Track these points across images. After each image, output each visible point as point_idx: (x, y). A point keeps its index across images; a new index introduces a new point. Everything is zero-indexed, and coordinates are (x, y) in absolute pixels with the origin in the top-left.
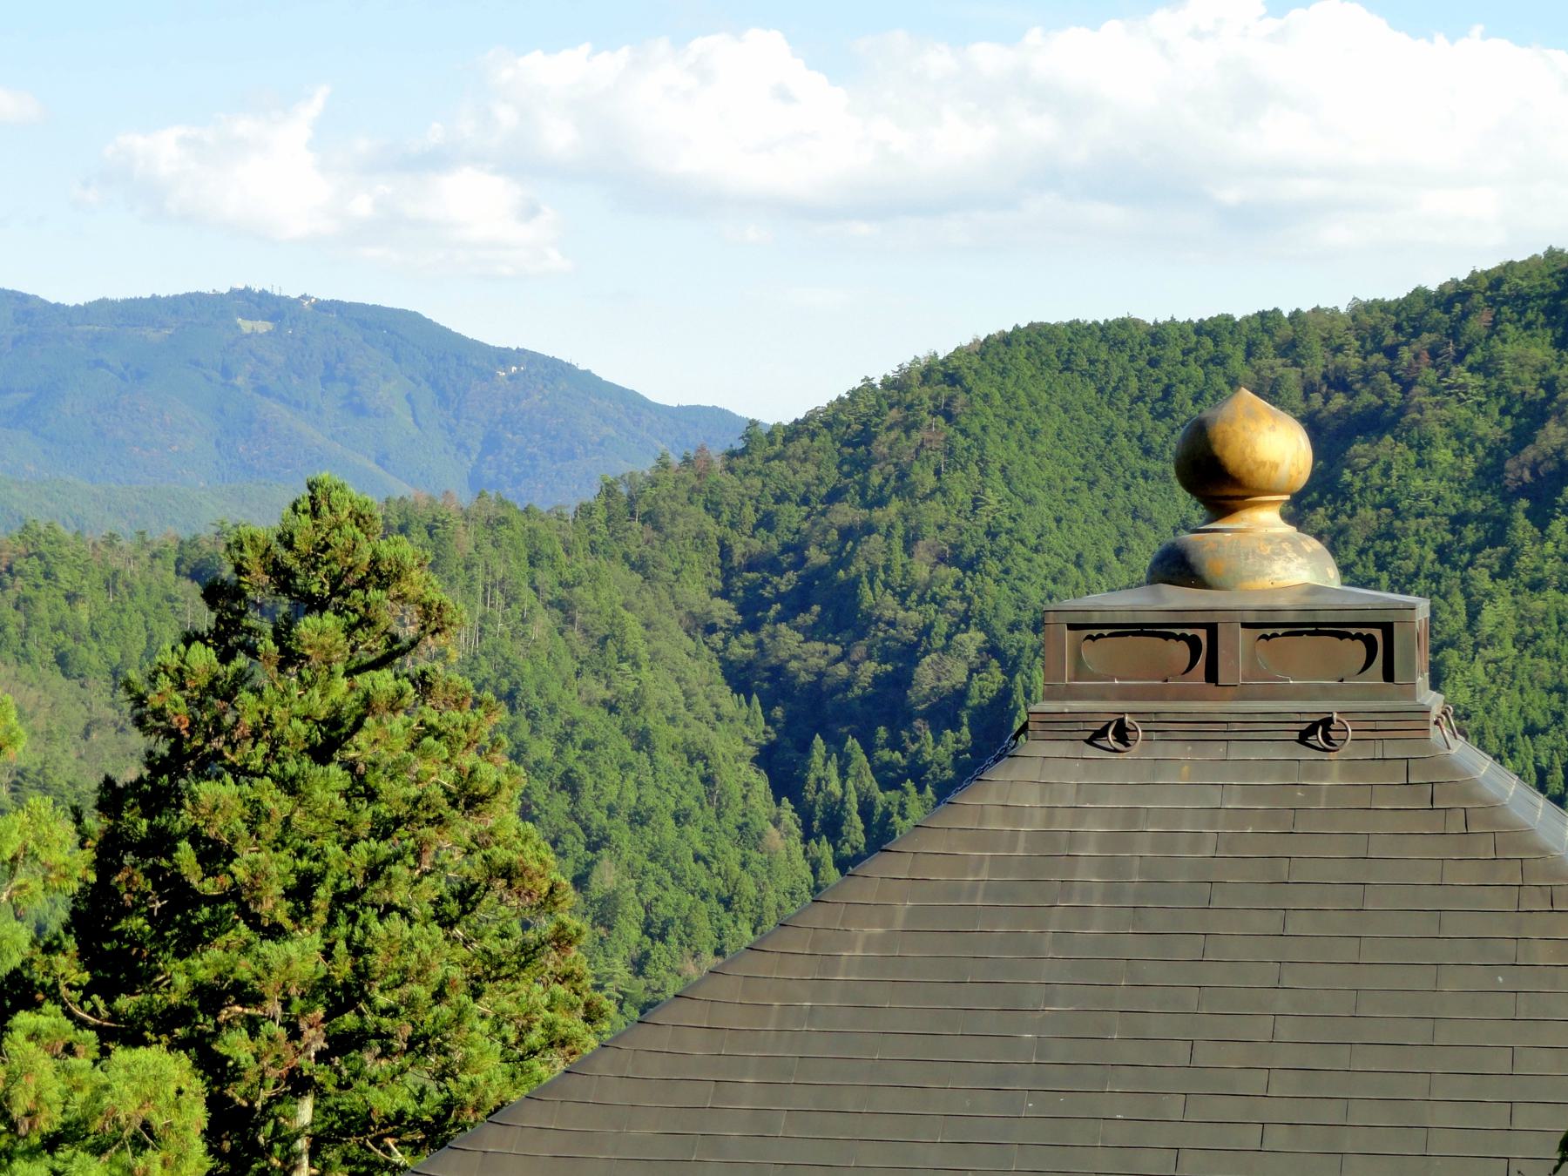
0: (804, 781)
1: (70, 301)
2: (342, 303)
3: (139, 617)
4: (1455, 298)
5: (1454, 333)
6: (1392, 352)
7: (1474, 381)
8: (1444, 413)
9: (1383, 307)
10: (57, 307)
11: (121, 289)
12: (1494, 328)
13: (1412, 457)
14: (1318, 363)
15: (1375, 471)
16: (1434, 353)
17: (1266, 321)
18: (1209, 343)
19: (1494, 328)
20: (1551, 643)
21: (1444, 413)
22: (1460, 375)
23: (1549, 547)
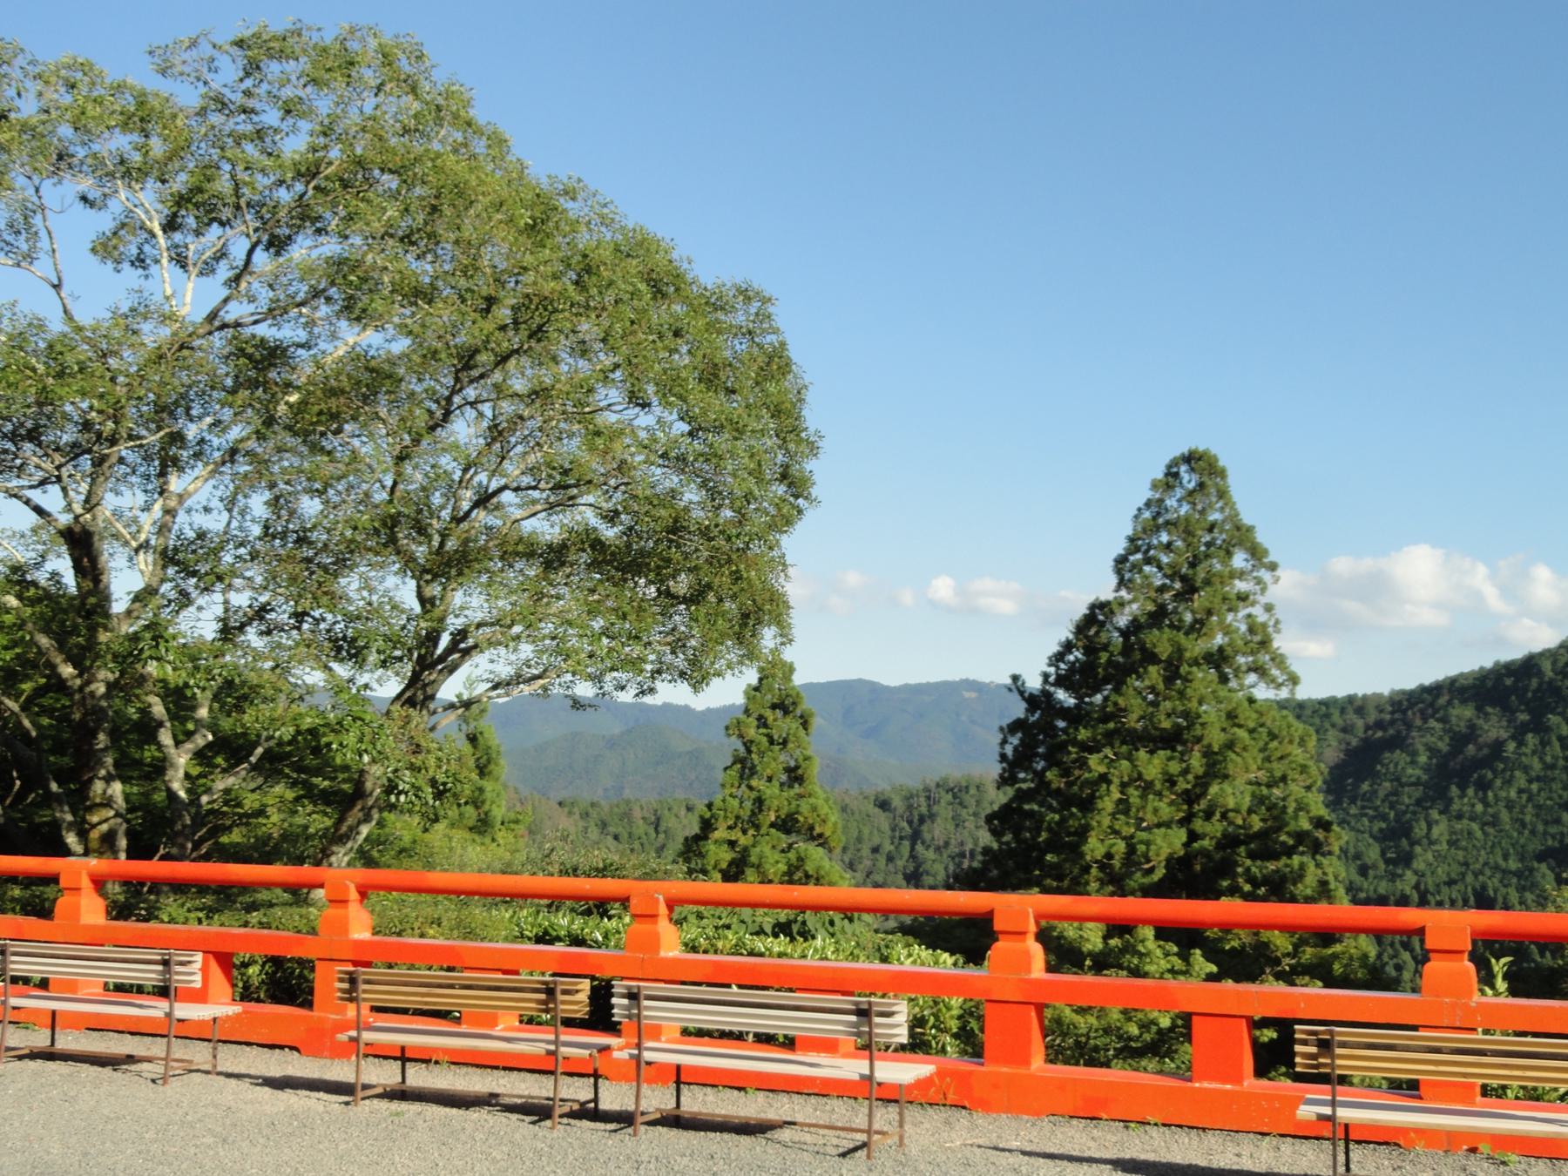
0: (1551, 969)
1: (893, 684)
2: (874, 691)
3: (855, 824)
4: (1434, 690)
5: (1432, 705)
6: (1404, 712)
7: (1438, 726)
8: (1424, 740)
9: (1403, 692)
10: (887, 687)
11: (913, 680)
12: (1449, 703)
13: (1408, 759)
14: (1372, 717)
15: (1392, 766)
16: (1422, 712)
17: (1351, 699)
18: (1324, 708)
19: (1449, 703)
20: (1464, 843)
21: (1424, 740)
22: (1432, 723)
23: (1466, 800)
